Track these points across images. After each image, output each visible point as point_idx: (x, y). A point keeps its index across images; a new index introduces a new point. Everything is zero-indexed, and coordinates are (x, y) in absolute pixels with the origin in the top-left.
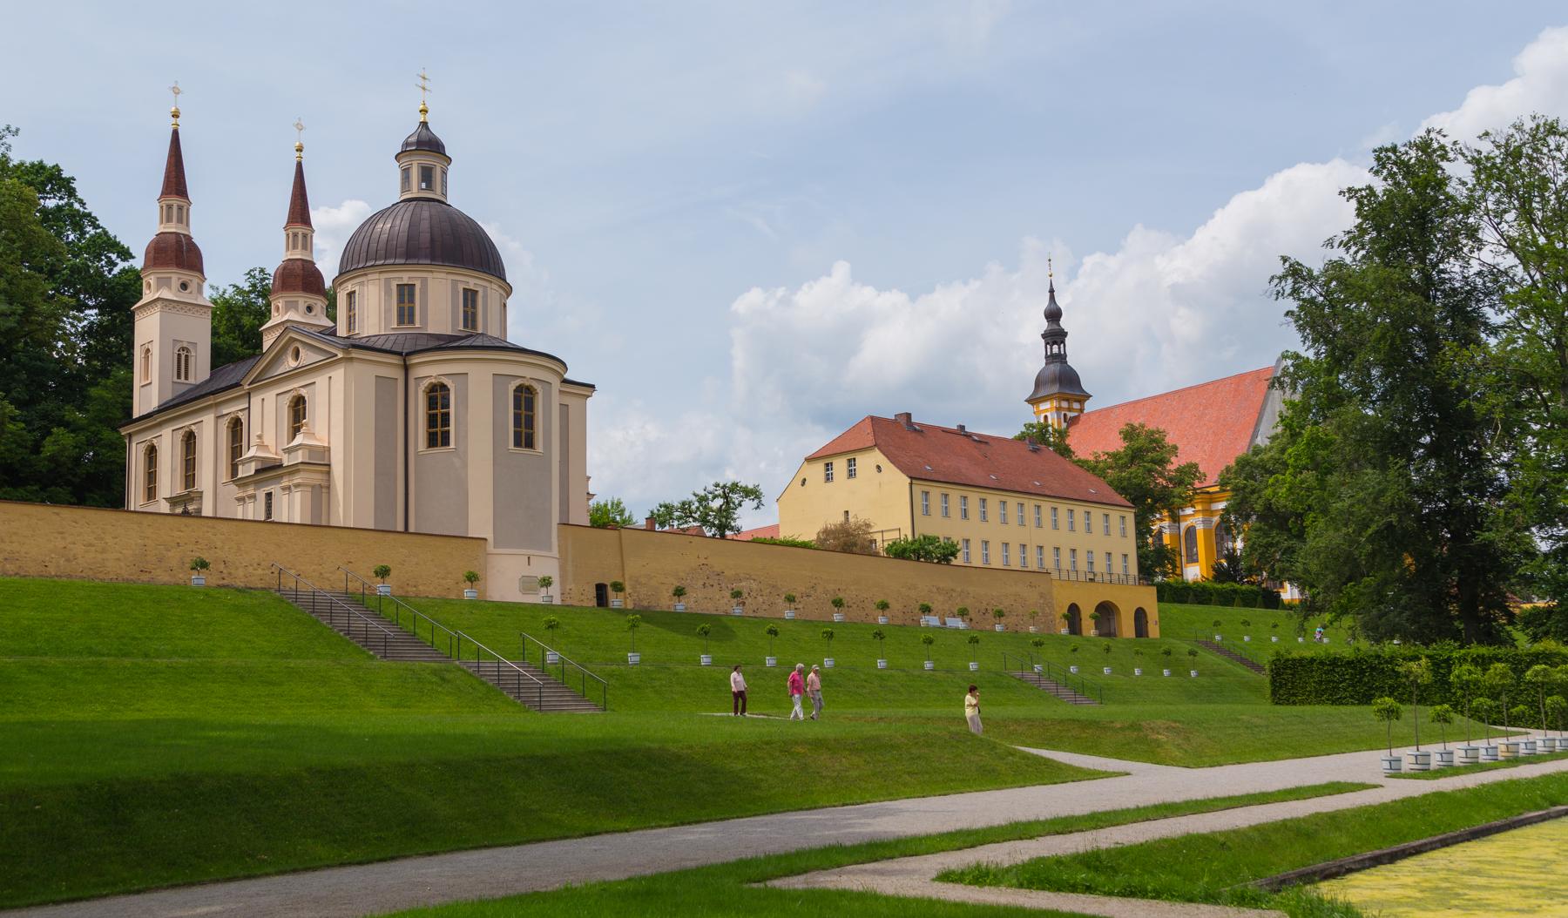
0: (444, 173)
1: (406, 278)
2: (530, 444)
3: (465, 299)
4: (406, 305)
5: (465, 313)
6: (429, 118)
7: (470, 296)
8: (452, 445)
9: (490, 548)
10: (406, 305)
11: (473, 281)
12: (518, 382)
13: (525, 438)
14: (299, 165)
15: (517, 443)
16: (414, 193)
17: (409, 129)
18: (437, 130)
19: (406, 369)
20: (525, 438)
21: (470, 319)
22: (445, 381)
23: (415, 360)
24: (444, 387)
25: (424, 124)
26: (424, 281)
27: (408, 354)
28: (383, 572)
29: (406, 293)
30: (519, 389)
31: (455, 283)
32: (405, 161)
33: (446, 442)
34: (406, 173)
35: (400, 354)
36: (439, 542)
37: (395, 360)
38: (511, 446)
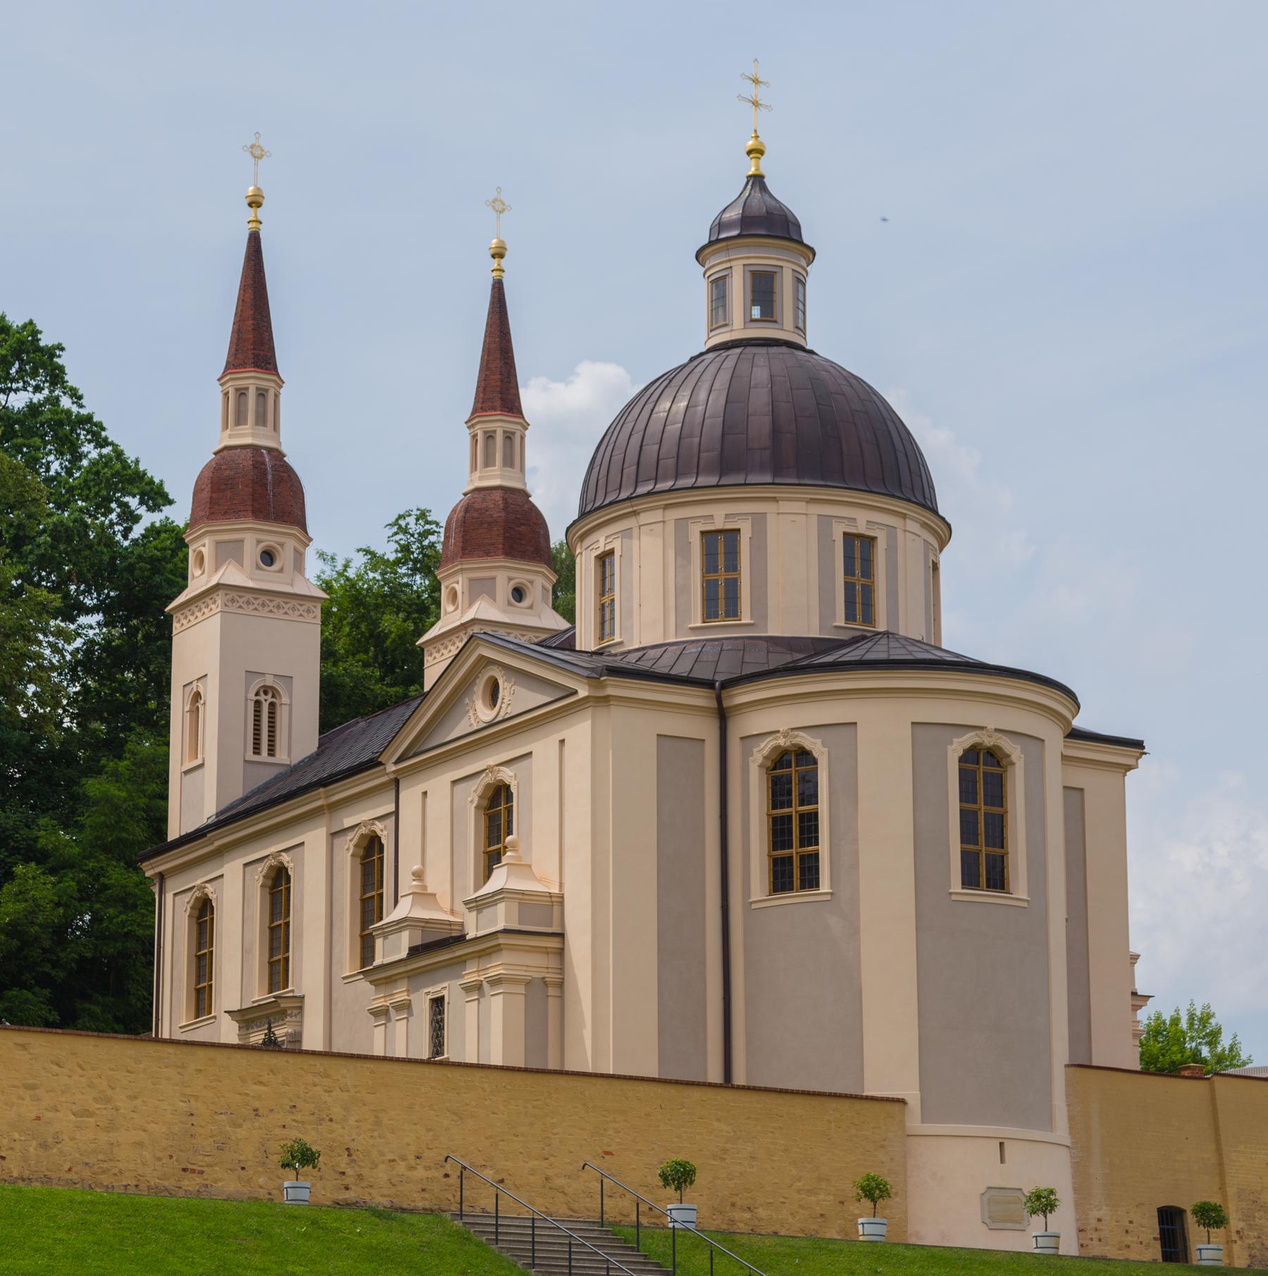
0: (800, 282)
1: (719, 516)
6: (766, 166)
7: (859, 550)
8: (825, 887)
9: (914, 1121)
10: (722, 577)
17: (724, 194)
18: (784, 191)
19: (723, 716)
23: (742, 696)
24: (804, 756)
25: (757, 180)
26: (759, 521)
32: (717, 262)
33: (810, 880)
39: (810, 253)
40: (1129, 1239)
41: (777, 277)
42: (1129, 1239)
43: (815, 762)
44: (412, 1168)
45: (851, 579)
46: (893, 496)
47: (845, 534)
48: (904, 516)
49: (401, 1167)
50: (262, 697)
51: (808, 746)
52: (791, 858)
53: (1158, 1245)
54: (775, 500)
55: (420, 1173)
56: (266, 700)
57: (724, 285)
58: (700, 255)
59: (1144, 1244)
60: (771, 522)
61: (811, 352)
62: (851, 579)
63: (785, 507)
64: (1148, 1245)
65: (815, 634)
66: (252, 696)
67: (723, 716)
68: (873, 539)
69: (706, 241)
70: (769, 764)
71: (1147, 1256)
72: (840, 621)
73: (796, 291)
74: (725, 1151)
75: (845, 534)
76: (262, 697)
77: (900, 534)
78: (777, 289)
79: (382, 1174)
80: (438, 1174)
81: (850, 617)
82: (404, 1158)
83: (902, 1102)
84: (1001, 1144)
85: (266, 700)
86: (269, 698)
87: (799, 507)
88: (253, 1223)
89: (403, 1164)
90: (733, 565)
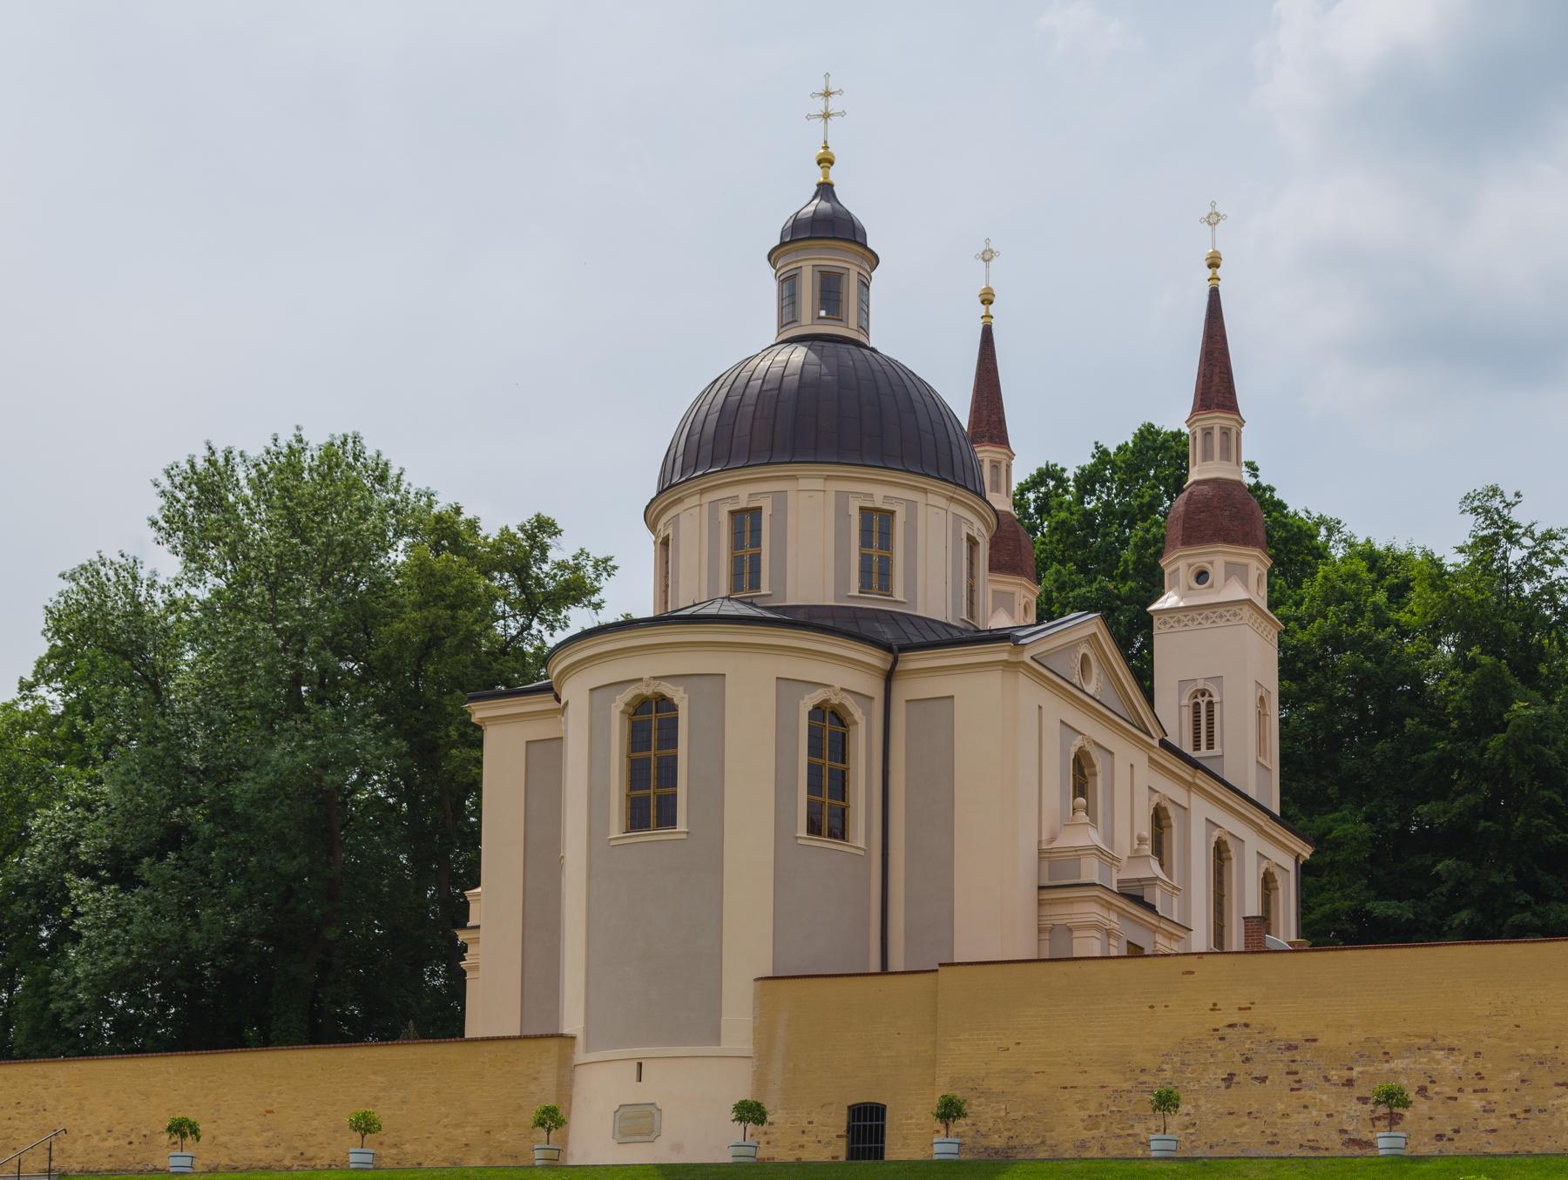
0: (865, 285)
1: (743, 496)
2: (840, 832)
3: (866, 532)
4: (875, 552)
5: (865, 560)
6: (835, 175)
7: (877, 525)
8: (682, 825)
9: (580, 1055)
10: (747, 552)
11: (882, 490)
12: (629, 693)
13: (828, 820)
14: (987, 334)
15: (814, 828)
16: (807, 326)
17: (800, 200)
18: (850, 199)
19: (889, 677)
20: (828, 820)
21: (877, 573)
22: (667, 689)
23: (913, 661)
24: (664, 704)
25: (825, 190)
26: (780, 498)
27: (904, 649)
28: (182, 1129)
29: (877, 525)
30: (818, 712)
31: (842, 498)
32: (788, 263)
33: (667, 818)
34: (789, 286)
35: (887, 648)
36: (502, 1045)
37: (875, 658)
38: (802, 831)
39: (874, 260)
40: (804, 1139)
41: (844, 279)
42: (804, 1139)
43: (674, 708)
44: (105, 1140)
45: (884, 553)
46: (928, 475)
47: (861, 508)
48: (925, 491)
49: (95, 1140)
50: (1200, 699)
51: (669, 694)
52: (648, 797)
53: (843, 1143)
54: (795, 478)
55: (111, 1142)
56: (1203, 701)
57: (794, 284)
58: (773, 256)
59: (827, 1141)
60: (791, 496)
61: (873, 350)
62: (884, 553)
63: (932, 499)
64: (829, 1143)
65: (830, 602)
66: (1185, 701)
67: (889, 677)
68: (893, 513)
69: (777, 242)
70: (631, 710)
71: (824, 1155)
72: (855, 590)
73: (860, 293)
74: (377, 1099)
75: (861, 508)
76: (1200, 699)
77: (921, 509)
78: (844, 291)
79: (79, 1146)
80: (124, 1142)
81: (865, 586)
82: (97, 1133)
83: (573, 1038)
84: (640, 1065)
85: (1203, 701)
86: (1206, 699)
87: (818, 484)
88: (970, 1084)
89: (96, 1138)
90: (756, 541)
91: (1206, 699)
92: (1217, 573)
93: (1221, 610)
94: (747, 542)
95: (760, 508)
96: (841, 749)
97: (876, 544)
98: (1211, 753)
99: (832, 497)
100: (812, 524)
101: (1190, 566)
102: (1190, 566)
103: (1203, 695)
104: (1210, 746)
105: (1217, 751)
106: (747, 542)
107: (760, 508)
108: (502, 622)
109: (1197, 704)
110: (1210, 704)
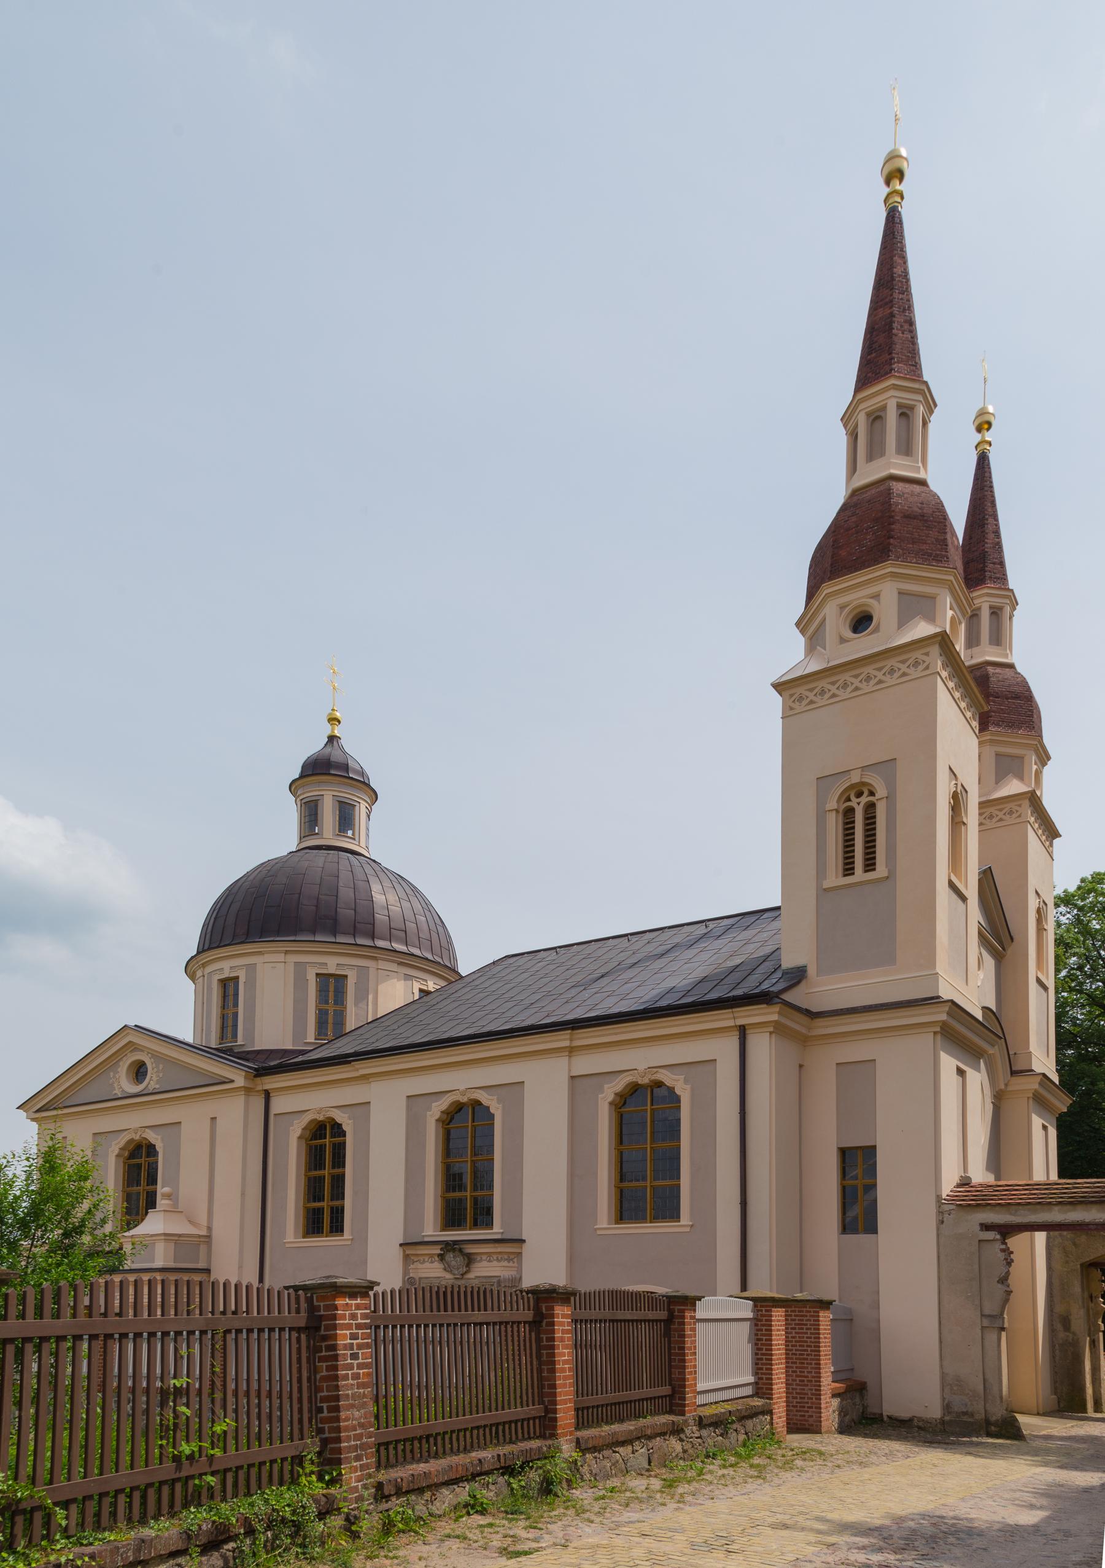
3: (322, 991)
4: (331, 1008)
26: (251, 968)
31: (300, 968)
54: (260, 953)
66: (832, 804)
76: (853, 803)
86: (864, 799)
87: (281, 957)
91: (864, 799)
92: (886, 610)
93: (892, 662)
94: (231, 1004)
95: (237, 978)
96: (313, 1189)
97: (331, 1013)
98: (871, 875)
99: (291, 968)
100: (278, 993)
101: (842, 608)
102: (842, 608)
103: (859, 794)
104: (870, 864)
105: (881, 870)
106: (231, 1004)
107: (237, 978)
108: (32, 1188)
109: (849, 812)
110: (871, 807)
